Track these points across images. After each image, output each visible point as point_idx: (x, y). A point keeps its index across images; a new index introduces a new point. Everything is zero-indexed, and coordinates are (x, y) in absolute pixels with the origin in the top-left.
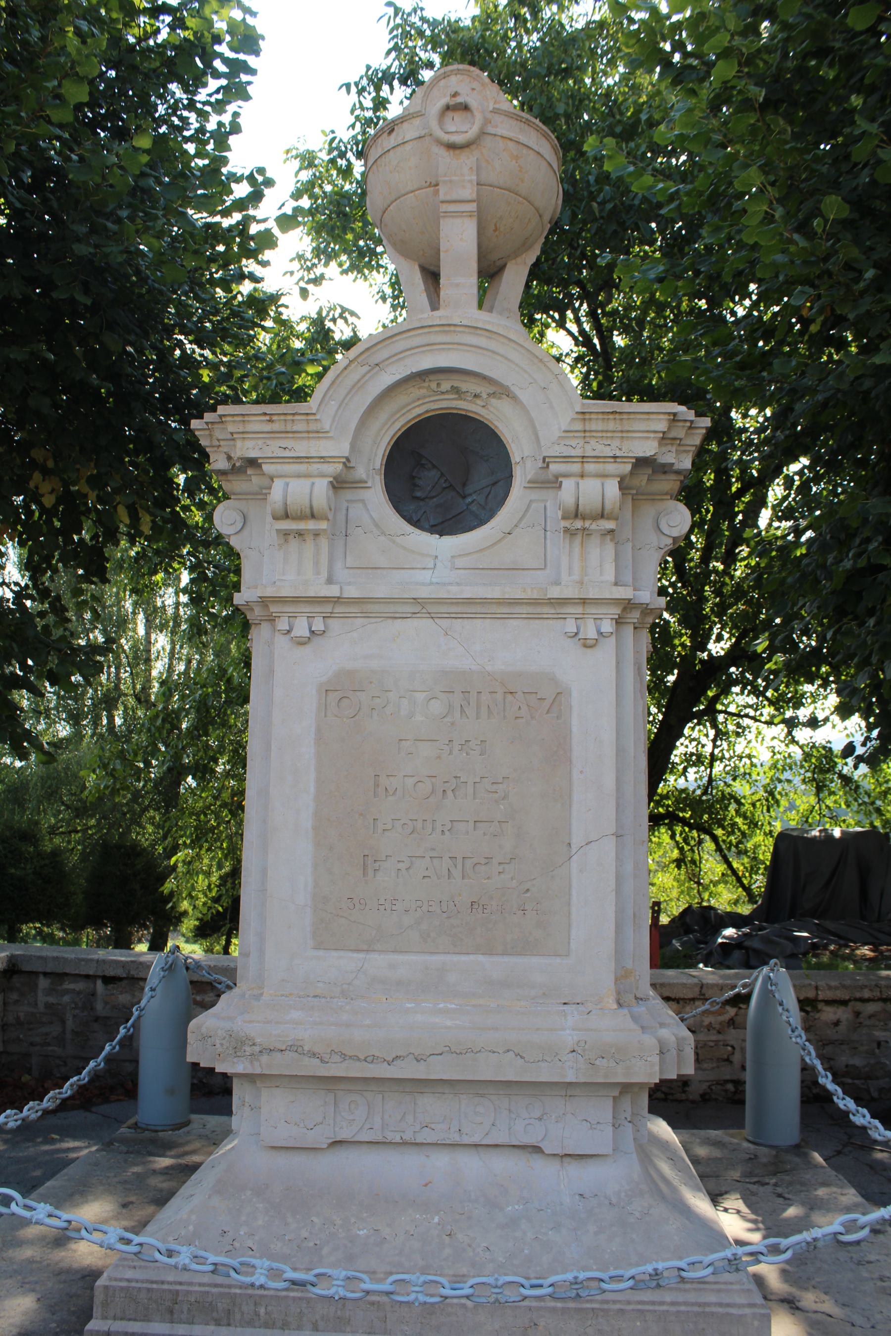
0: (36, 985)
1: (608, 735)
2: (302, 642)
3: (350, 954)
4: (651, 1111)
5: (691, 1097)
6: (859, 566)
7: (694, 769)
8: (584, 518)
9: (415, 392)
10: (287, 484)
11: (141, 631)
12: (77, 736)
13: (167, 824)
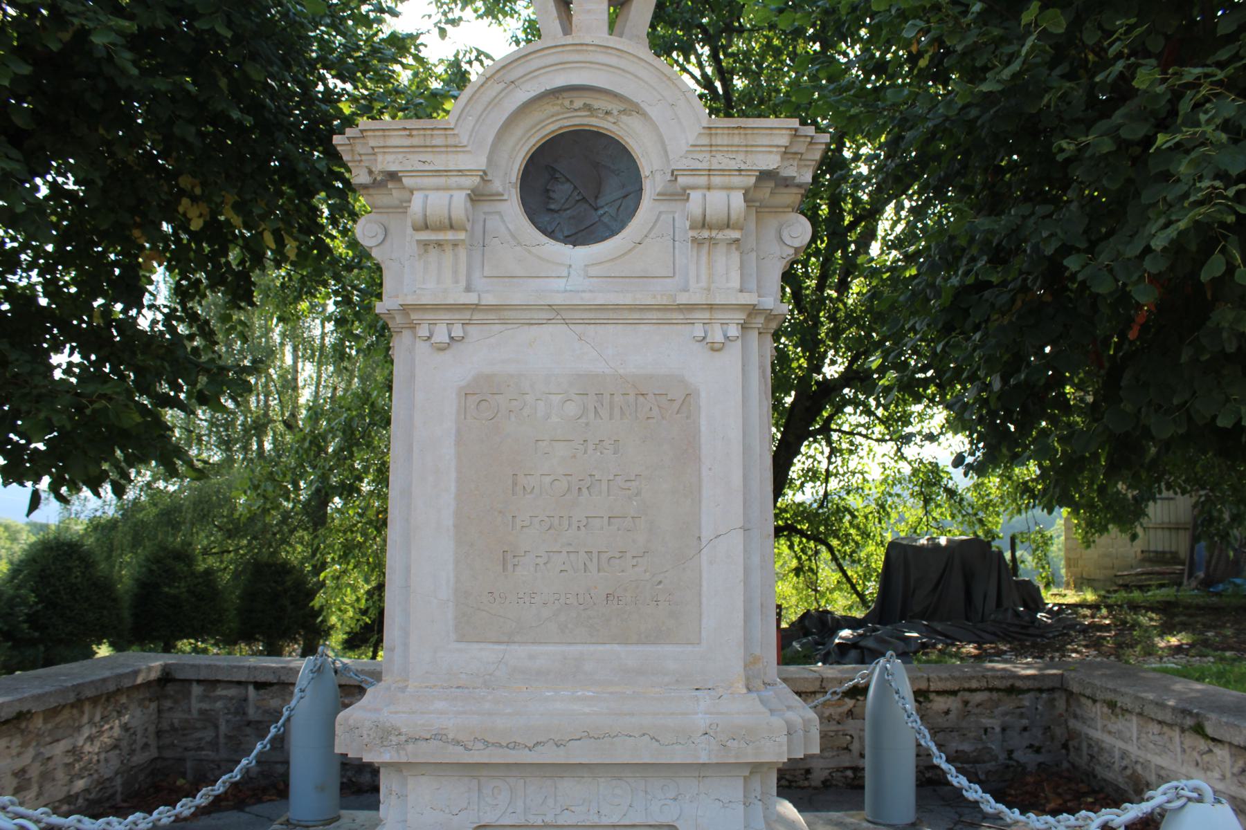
0: (190, 693)
1: (735, 434)
2: (442, 348)
3: (491, 646)
4: (780, 794)
5: (813, 784)
6: (967, 282)
7: (811, 484)
8: (710, 228)
9: (550, 108)
10: (427, 197)
11: (289, 360)
12: (229, 461)
13: (316, 542)
